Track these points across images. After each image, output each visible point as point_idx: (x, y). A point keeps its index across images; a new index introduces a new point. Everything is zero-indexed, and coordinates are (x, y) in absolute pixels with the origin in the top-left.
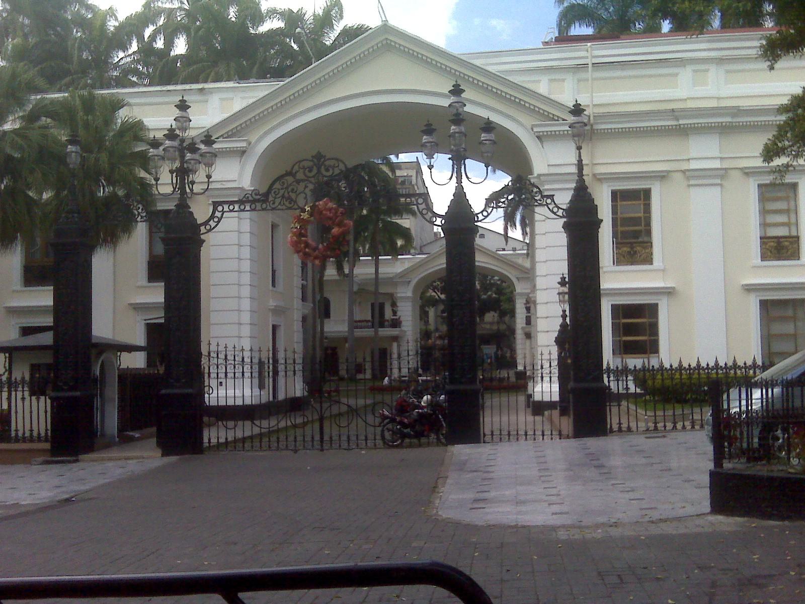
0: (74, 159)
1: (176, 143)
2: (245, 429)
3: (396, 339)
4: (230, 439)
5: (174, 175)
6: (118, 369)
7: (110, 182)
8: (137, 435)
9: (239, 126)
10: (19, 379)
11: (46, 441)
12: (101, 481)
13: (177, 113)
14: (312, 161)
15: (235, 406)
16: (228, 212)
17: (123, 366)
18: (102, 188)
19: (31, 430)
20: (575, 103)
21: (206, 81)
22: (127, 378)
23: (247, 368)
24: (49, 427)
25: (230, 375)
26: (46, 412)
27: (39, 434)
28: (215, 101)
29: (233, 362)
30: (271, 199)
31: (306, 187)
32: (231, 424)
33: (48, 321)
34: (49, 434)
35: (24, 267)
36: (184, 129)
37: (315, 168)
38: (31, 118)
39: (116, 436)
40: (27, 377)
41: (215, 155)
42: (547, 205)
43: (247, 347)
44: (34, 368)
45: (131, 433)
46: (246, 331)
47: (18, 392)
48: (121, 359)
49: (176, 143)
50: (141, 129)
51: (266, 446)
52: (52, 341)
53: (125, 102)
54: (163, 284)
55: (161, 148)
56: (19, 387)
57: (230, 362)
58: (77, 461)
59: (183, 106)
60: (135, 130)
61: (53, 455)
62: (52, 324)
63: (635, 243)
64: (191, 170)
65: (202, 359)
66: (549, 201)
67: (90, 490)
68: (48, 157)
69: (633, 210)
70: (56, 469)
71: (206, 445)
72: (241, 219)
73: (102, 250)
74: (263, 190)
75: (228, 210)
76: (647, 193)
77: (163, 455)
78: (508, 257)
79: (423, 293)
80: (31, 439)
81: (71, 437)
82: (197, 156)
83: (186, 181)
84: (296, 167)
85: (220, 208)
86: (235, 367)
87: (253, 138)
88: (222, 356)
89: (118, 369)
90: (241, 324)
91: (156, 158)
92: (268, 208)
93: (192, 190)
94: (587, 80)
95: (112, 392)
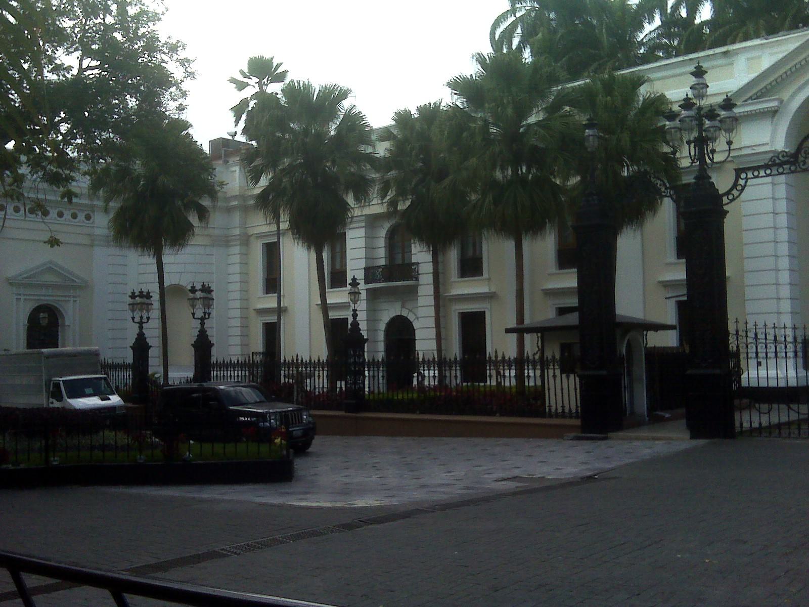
0: (592, 143)
1: (691, 113)
2: (780, 414)
5: (692, 145)
6: (645, 348)
7: (633, 160)
8: (667, 415)
9: (765, 87)
10: (550, 357)
11: (577, 417)
12: (627, 461)
13: (693, 80)
15: (749, 387)
16: (752, 178)
17: (651, 344)
18: (626, 168)
19: (563, 407)
20: (686, 97)
21: (734, 42)
22: (656, 356)
23: (791, 347)
24: (579, 405)
25: (771, 355)
26: (576, 389)
27: (570, 410)
28: (741, 62)
29: (764, 341)
30: (801, 158)
32: (765, 407)
33: (573, 302)
34: (579, 411)
35: (266, 279)
36: (701, 96)
38: (553, 109)
39: (646, 416)
40: (558, 357)
41: (736, 120)
43: (789, 324)
44: (564, 348)
45: (663, 414)
46: (786, 306)
47: (430, 371)
48: (647, 337)
49: (691, 113)
50: (663, 103)
51: (785, 434)
52: (578, 320)
53: (646, 78)
54: (576, 270)
55: (677, 120)
56: (550, 365)
57: (761, 341)
58: (606, 438)
59: (699, 73)
60: (657, 104)
61: (583, 432)
62: (577, 305)
64: (710, 139)
65: (730, 338)
67: (612, 469)
68: (569, 144)
70: (588, 445)
71: (738, 429)
72: (775, 184)
73: (629, 229)
74: (791, 150)
75: (752, 176)
77: (692, 438)
80: (563, 415)
81: (600, 416)
82: (717, 123)
83: (706, 152)
85: (743, 176)
86: (766, 347)
87: (785, 96)
88: (751, 335)
89: (645, 348)
90: (780, 299)
91: (673, 130)
92: (798, 169)
93: (712, 160)
95: (640, 370)
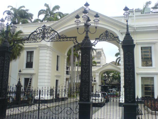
3: (95, 84)
4: (11, 114)
14: (42, 28)
30: (30, 39)
31: (40, 35)
37: (43, 30)
42: (116, 40)
63: (147, 61)
66: (117, 39)
69: (148, 83)
76: (151, 47)
78: (119, 67)
79: (102, 75)
84: (37, 30)
94: (136, 25)
